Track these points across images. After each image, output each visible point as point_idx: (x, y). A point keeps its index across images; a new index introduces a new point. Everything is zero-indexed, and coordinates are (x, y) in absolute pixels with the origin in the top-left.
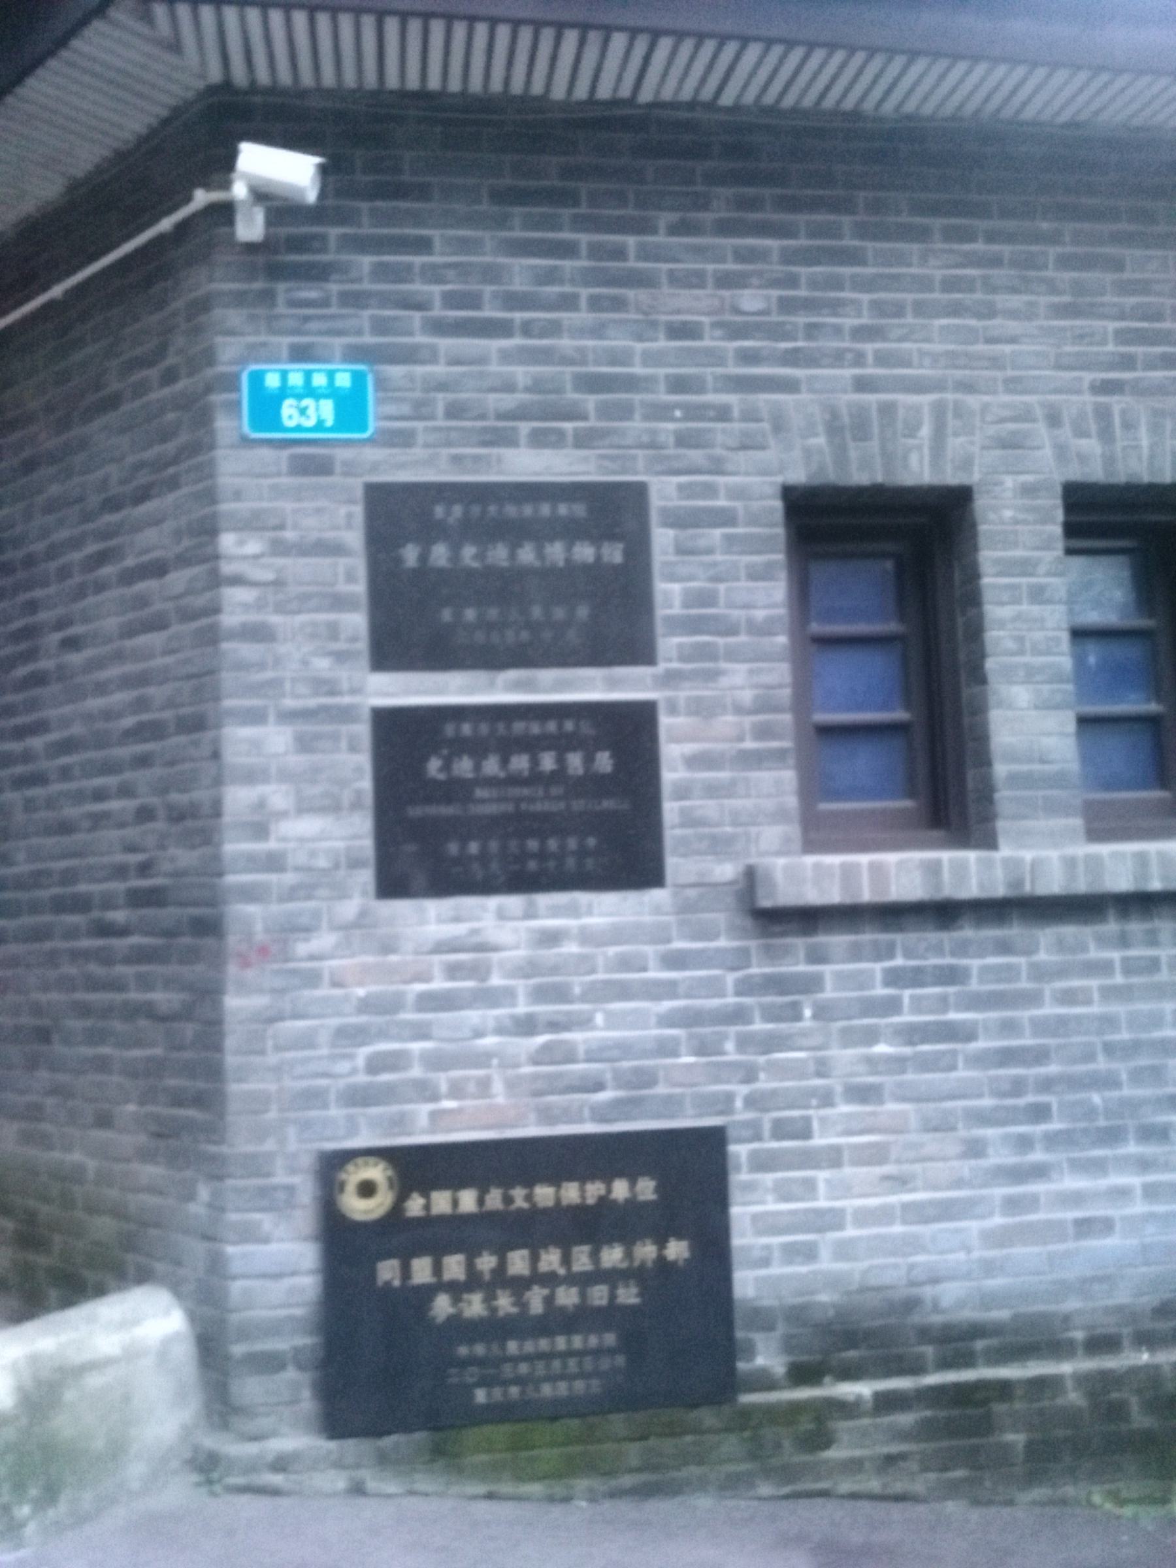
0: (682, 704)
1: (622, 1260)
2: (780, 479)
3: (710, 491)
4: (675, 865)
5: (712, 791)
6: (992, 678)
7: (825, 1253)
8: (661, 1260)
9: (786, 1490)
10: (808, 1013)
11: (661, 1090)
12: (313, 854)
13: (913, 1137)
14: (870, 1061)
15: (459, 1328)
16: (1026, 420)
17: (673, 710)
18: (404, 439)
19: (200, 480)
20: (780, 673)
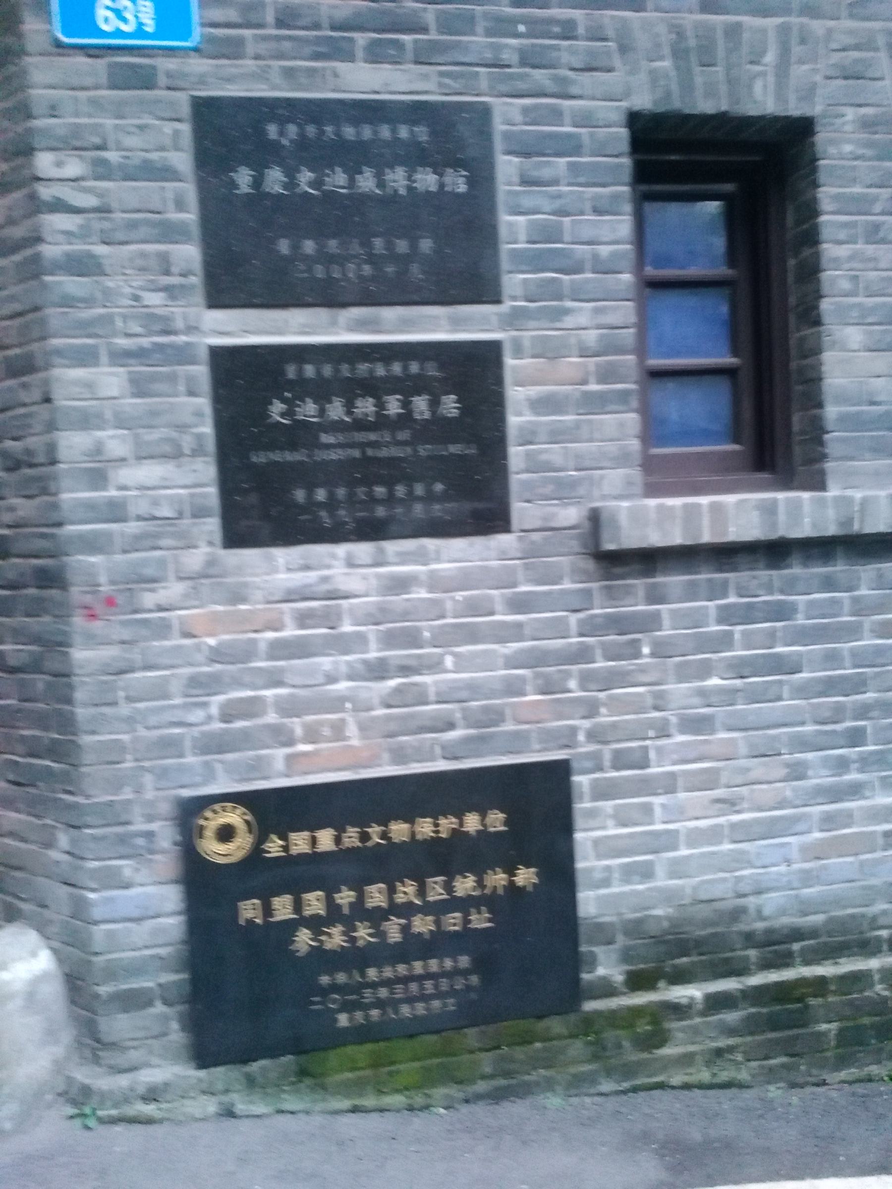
0: (527, 343)
1: (474, 889)
2: (624, 104)
3: (556, 115)
4: (521, 510)
5: (557, 436)
6: (827, 318)
7: (660, 871)
8: (512, 887)
9: (626, 1085)
10: (646, 650)
11: (509, 727)
12: (155, 502)
13: (743, 762)
14: (702, 692)
15: (322, 958)
16: (869, 50)
17: (518, 352)
18: (230, 49)
19: (10, 94)
20: (624, 312)
